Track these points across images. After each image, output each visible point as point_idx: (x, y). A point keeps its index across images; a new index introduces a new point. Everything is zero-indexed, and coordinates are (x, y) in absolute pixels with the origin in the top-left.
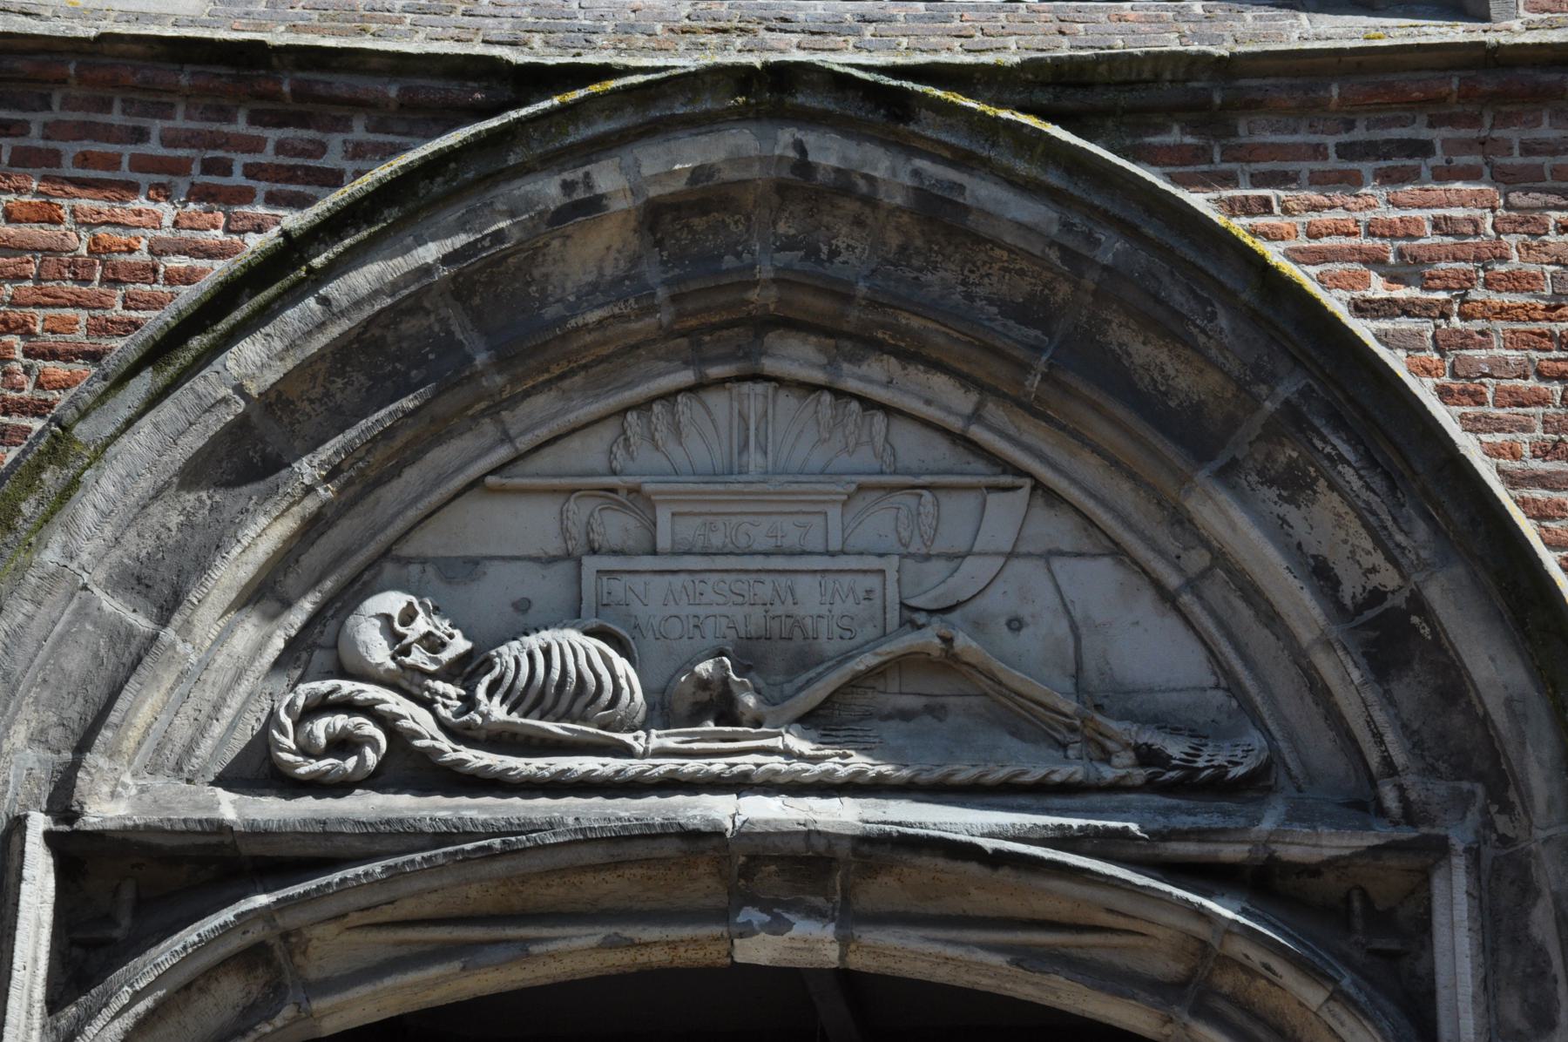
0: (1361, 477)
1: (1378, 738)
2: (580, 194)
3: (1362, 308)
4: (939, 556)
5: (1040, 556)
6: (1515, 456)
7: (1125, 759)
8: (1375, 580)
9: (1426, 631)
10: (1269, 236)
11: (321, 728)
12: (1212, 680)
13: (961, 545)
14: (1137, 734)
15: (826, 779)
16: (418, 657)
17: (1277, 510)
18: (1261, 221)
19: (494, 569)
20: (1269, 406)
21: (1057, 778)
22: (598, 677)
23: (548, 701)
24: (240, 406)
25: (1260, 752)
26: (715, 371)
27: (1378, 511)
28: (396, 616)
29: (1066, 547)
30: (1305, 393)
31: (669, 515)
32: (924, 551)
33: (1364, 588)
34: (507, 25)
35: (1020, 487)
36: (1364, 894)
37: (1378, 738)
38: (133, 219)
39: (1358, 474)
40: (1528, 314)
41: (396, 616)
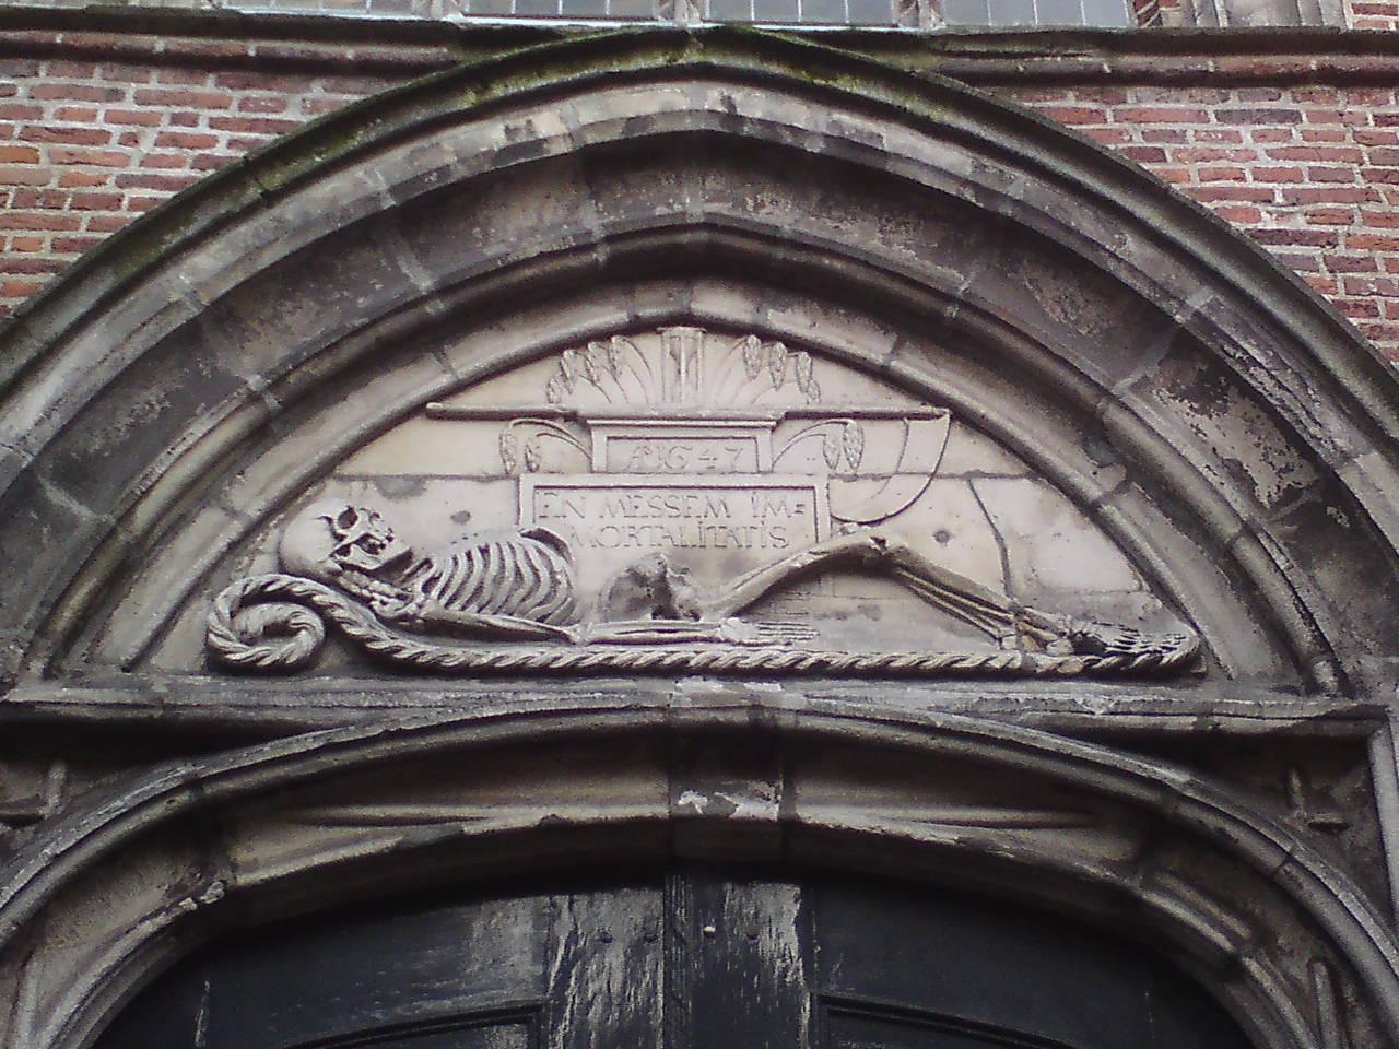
0: (1273, 377)
1: (1308, 617)
2: (521, 138)
4: (865, 477)
5: (961, 477)
7: (1064, 645)
9: (1343, 521)
11: (259, 616)
13: (889, 468)
14: (1071, 622)
16: (357, 556)
17: (1189, 420)
21: (996, 664)
22: (535, 571)
23: (486, 595)
25: (1191, 639)
27: (1292, 407)
28: (335, 518)
31: (605, 439)
32: (851, 472)
33: (1279, 488)
35: (938, 417)
37: (1308, 617)
39: (1270, 374)
41: (335, 518)
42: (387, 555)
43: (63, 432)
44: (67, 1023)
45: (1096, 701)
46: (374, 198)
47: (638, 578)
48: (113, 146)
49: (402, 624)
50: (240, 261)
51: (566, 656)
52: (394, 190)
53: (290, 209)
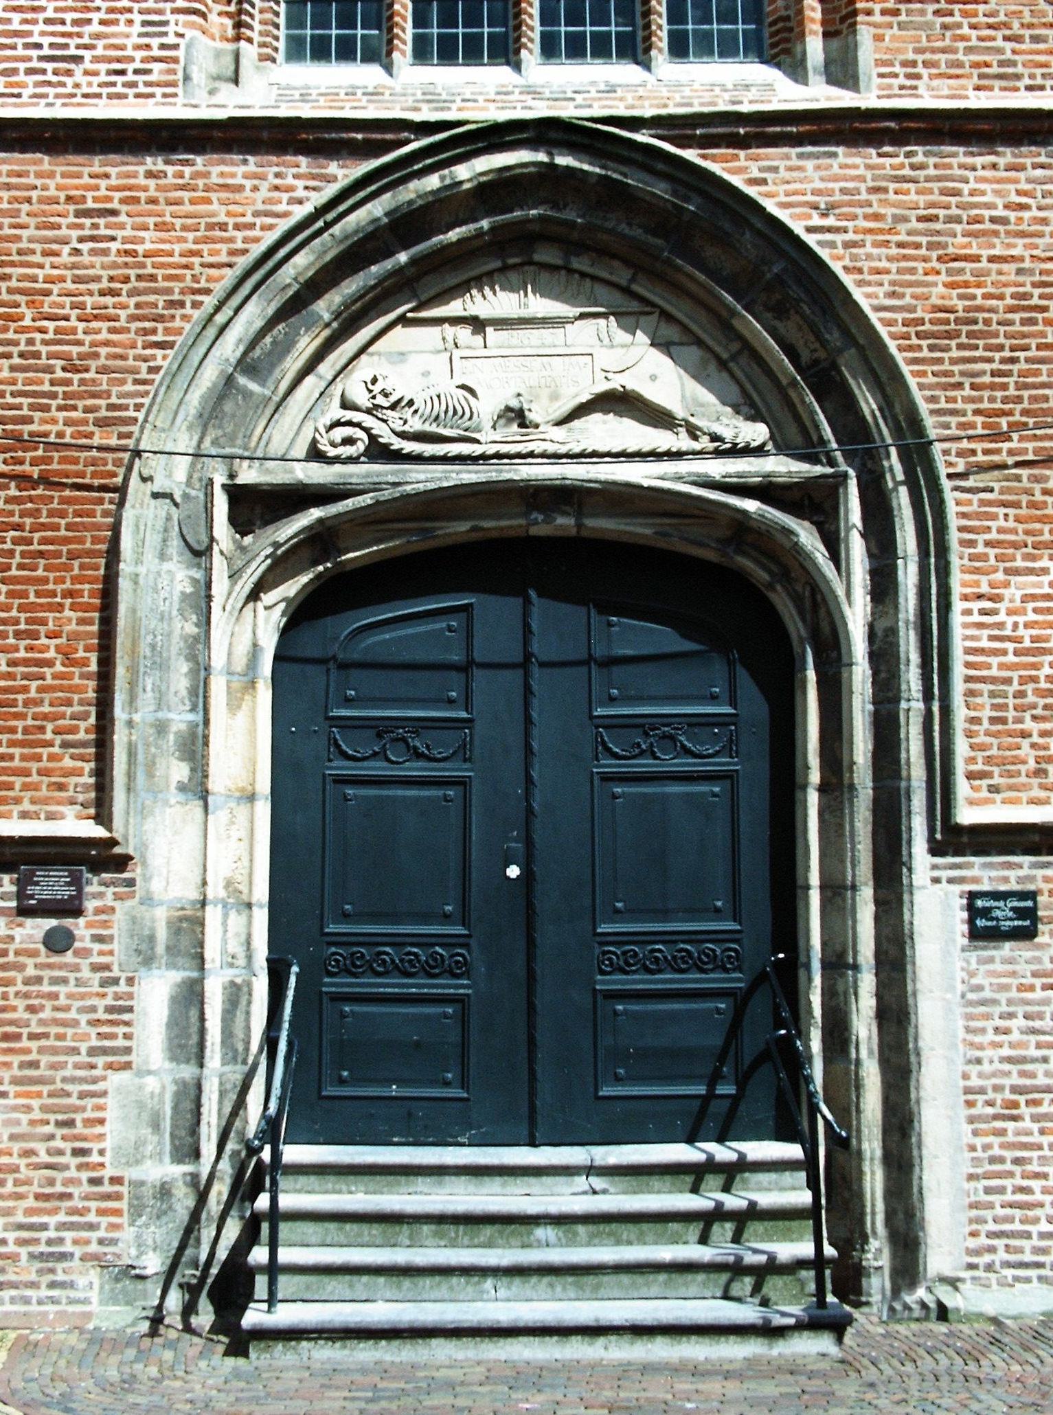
2: (448, 182)
3: (810, 230)
6: (877, 297)
7: (706, 438)
8: (816, 355)
10: (768, 195)
11: (339, 433)
12: (742, 401)
15: (271, 1343)
16: (380, 400)
18: (763, 189)
19: (412, 358)
20: (768, 276)
24: (296, 287)
26: (511, 261)
29: (677, 340)
30: (785, 270)
34: (411, 99)
36: (810, 498)
38: (244, 201)
40: (881, 231)
42: (393, 399)
43: (245, 354)
44: (164, 541)
45: (717, 468)
46: (377, 220)
47: (508, 409)
48: (248, 193)
49: (403, 435)
50: (316, 259)
51: (477, 450)
52: (386, 214)
53: (336, 229)
